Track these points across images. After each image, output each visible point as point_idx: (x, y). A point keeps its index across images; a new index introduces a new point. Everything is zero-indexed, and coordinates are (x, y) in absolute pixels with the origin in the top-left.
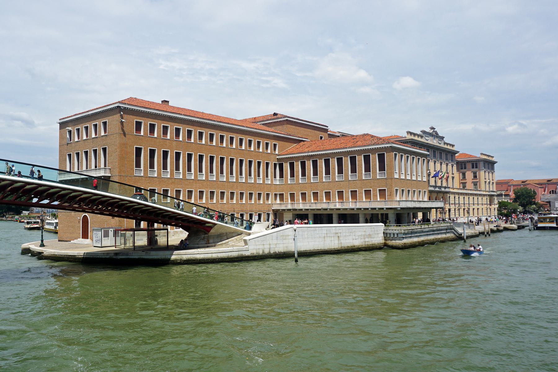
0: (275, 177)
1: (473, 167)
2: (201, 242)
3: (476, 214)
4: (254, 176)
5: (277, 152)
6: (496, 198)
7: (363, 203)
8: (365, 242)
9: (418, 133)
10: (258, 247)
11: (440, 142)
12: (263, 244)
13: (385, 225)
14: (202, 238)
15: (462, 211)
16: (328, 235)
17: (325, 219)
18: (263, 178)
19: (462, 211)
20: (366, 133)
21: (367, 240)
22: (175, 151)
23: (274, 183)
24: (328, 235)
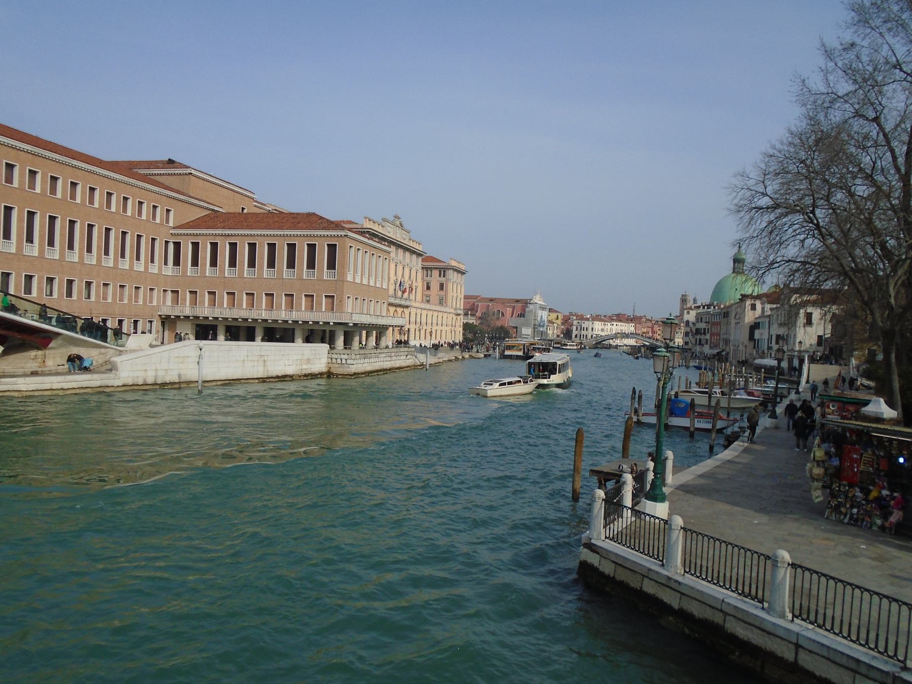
0: (166, 263)
1: (440, 276)
2: (30, 364)
3: (417, 338)
4: (130, 258)
5: (171, 224)
6: (643, 348)
7: (301, 314)
8: (302, 369)
9: (379, 222)
10: (136, 374)
11: (404, 236)
12: (144, 369)
13: (330, 347)
14: (32, 357)
15: (423, 332)
16: (250, 358)
17: (242, 334)
18: (146, 263)
19: (423, 332)
20: (311, 211)
21: (304, 367)
22: (26, 209)
23: (163, 273)
24: (250, 358)
